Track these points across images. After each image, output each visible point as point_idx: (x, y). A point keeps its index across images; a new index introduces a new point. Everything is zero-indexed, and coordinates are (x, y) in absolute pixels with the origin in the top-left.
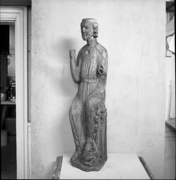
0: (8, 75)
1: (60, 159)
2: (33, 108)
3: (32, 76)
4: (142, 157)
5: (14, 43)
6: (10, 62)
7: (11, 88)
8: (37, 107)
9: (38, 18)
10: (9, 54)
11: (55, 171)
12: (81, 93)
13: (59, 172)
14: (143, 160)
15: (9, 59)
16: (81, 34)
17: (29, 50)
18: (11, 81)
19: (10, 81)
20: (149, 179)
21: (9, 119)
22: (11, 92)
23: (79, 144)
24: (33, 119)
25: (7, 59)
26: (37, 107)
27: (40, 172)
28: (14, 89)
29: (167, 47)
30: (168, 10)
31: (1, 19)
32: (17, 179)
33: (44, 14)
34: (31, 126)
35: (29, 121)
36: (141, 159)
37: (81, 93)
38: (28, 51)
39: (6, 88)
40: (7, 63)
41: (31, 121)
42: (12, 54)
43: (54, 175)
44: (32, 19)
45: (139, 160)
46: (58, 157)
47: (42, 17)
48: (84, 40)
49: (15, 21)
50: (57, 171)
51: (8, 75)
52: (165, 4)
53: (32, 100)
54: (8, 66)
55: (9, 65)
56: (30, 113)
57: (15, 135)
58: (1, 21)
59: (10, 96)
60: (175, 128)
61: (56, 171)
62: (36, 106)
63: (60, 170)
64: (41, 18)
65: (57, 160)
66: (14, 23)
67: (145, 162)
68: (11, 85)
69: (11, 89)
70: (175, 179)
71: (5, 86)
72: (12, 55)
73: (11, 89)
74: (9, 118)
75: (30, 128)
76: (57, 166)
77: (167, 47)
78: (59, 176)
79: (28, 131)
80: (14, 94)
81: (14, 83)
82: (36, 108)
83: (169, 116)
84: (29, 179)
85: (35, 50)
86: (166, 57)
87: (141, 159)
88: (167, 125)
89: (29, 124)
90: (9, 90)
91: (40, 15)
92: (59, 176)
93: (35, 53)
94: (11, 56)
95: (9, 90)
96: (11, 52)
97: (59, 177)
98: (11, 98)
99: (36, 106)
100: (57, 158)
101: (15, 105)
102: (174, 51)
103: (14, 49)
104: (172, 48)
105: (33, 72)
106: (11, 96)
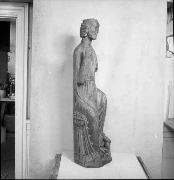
1: (58, 157)
4: (140, 157)
11: (53, 169)
20: (147, 179)
36: (139, 159)
43: (52, 173)
63: (58, 167)
78: (57, 174)
92: (57, 174)
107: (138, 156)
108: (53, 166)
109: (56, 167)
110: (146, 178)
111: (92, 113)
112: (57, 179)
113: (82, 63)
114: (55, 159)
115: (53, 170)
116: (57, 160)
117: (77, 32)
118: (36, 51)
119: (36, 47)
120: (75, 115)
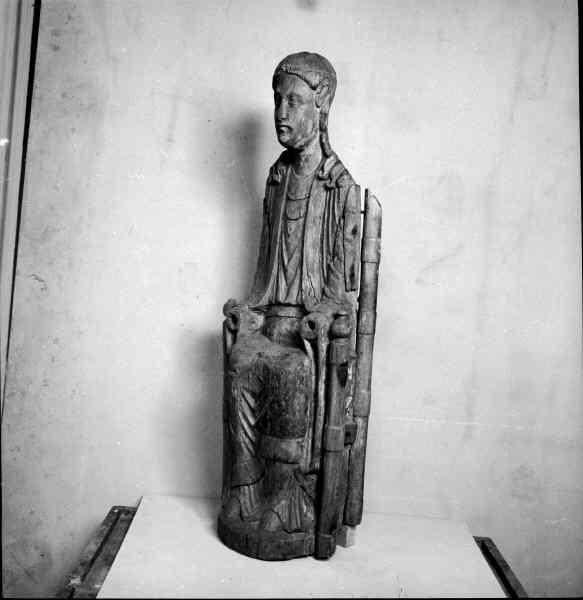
1: (123, 516)
4: (490, 541)
8: (41, 280)
11: (82, 564)
12: (322, 393)
13: (104, 570)
20: (505, 597)
26: (41, 280)
27: (29, 574)
36: (486, 547)
37: (322, 393)
43: (76, 581)
50: (95, 565)
61: (93, 561)
63: (109, 562)
76: (102, 544)
78: (97, 586)
92: (97, 586)
93: (56, 48)
97: (100, 588)
99: (37, 278)
100: (111, 512)
107: (483, 534)
108: (89, 552)
109: (99, 559)
110: (503, 595)
111: (298, 352)
112: (98, 597)
113: (322, 235)
114: (105, 523)
115: (80, 568)
116: (111, 530)
117: (264, 99)
118: (56, 48)
119: (56, 33)
120: (273, 429)
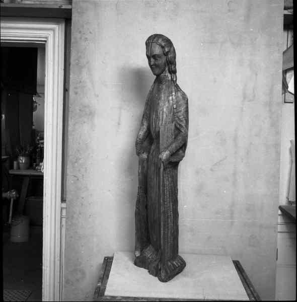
0: (33, 127)
2: (70, 181)
3: (70, 128)
5: (44, 75)
6: (36, 106)
7: (38, 148)
9: (81, 38)
10: (35, 93)
14: (241, 265)
15: (35, 102)
16: (281, 86)
17: (67, 87)
18: (38, 138)
19: (36, 138)
21: (32, 199)
22: (36, 155)
23: (159, 264)
24: (69, 197)
25: (33, 102)
28: (42, 151)
29: (285, 86)
30: (286, 27)
31: (1, 38)
32: (43, 300)
33: (90, 32)
34: (66, 208)
35: (63, 200)
38: (66, 90)
39: (29, 149)
40: (31, 107)
41: (67, 200)
42: (40, 93)
44: (73, 40)
45: (233, 266)
46: (105, 258)
47: (87, 37)
48: (155, 74)
49: (46, 41)
51: (33, 127)
52: (283, 18)
53: (68, 167)
54: (34, 113)
55: (35, 111)
56: (66, 188)
57: (40, 226)
58: (1, 41)
59: (35, 162)
60: (294, 215)
62: (75, 176)
63: (108, 277)
64: (86, 38)
65: (104, 261)
66: (44, 44)
67: (244, 269)
68: (39, 144)
69: (37, 150)
70: (295, 299)
71: (28, 145)
72: (40, 95)
73: (37, 150)
74: (33, 197)
75: (64, 212)
77: (285, 86)
79: (61, 215)
80: (41, 158)
81: (42, 141)
82: (76, 179)
83: (288, 198)
84: (61, 301)
85: (76, 88)
86: (285, 102)
87: (238, 263)
88: (284, 212)
89: (64, 205)
90: (34, 151)
91: (84, 34)
93: (76, 93)
94: (39, 96)
95: (34, 151)
96: (38, 90)
98: (36, 165)
100: (105, 259)
101: (42, 176)
102: (293, 92)
103: (43, 86)
104: (291, 88)
105: (71, 123)
106: (38, 160)
